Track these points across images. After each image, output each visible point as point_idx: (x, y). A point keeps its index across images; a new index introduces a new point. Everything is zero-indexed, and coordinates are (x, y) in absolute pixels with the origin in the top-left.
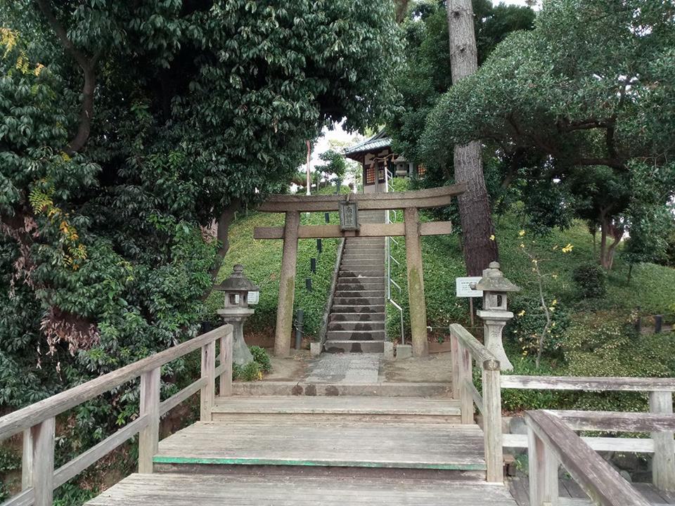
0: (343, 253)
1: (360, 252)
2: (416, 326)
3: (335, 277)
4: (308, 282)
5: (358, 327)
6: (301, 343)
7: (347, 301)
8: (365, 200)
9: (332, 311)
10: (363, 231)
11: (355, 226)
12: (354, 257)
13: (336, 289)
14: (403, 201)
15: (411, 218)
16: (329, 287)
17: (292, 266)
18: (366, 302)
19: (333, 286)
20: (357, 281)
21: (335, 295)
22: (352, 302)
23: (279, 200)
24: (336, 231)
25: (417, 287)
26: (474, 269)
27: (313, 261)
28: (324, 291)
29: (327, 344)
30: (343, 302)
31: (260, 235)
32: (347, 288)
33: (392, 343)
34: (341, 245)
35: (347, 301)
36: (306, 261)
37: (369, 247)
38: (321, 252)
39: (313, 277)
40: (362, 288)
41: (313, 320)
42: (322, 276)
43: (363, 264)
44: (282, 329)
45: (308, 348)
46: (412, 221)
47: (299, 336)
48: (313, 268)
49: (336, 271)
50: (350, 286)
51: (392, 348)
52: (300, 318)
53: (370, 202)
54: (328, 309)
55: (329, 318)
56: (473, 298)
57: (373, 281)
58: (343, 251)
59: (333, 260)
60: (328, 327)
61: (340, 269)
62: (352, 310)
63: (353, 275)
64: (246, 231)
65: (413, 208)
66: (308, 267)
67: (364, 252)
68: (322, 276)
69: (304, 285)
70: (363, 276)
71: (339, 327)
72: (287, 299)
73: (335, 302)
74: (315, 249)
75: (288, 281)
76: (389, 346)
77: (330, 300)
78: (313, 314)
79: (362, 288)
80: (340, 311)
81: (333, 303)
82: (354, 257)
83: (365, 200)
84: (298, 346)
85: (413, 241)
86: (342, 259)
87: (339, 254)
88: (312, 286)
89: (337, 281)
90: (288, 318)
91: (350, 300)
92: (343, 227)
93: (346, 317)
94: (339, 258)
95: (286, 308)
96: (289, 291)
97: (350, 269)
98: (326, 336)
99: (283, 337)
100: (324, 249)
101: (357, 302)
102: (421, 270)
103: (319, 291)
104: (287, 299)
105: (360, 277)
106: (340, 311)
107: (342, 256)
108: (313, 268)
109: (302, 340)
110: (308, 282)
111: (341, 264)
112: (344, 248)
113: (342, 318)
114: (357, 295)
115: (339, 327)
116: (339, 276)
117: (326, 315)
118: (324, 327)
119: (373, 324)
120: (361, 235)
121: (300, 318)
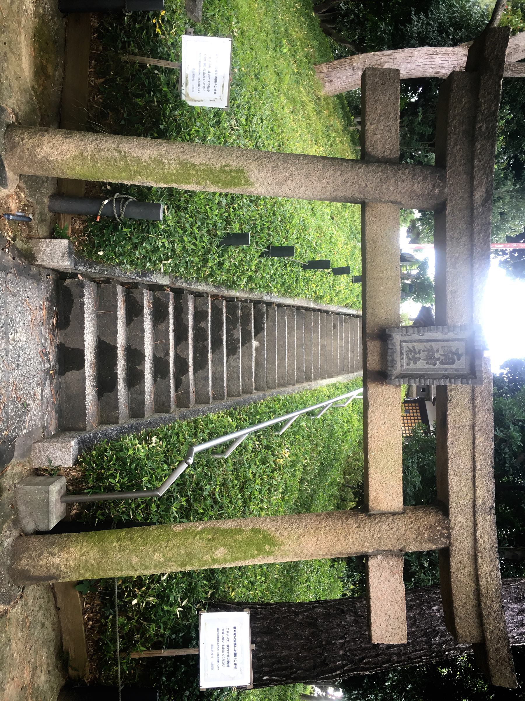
0: (299, 308)
1: (300, 339)
2: (104, 553)
3: (256, 295)
4: (240, 239)
5: (134, 355)
7: (203, 325)
8: (473, 399)
9: (179, 293)
12: (291, 329)
13: (230, 300)
14: (469, 510)
15: (420, 534)
16: (232, 285)
18: (200, 363)
19: (234, 293)
20: (246, 339)
21: (215, 297)
22: (200, 335)
23: (478, 145)
24: (380, 315)
27: (289, 251)
28: (222, 276)
29: (81, 285)
30: (199, 316)
31: (374, 90)
32: (232, 322)
34: (312, 305)
35: (203, 325)
36: (286, 238)
37: (308, 354)
38: (305, 267)
39: (254, 251)
40: (232, 350)
41: (135, 247)
42: (256, 271)
45: (54, 234)
49: (267, 298)
50: (235, 327)
51: (56, 463)
52: (137, 213)
53: (468, 414)
54: (181, 284)
55: (161, 288)
56: (198, 656)
57: (247, 370)
58: (302, 307)
59: (288, 291)
60: (135, 285)
61: (269, 304)
63: (258, 330)
64: (334, 137)
65: (449, 537)
66: (277, 241)
67: (300, 346)
68: (256, 271)
69: (236, 228)
70: (256, 350)
71: (134, 312)
72: (182, 164)
73: (200, 300)
74: (310, 256)
77: (202, 287)
78: (155, 250)
79: (232, 350)
80: (180, 311)
81: (198, 295)
82: (291, 329)
86: (288, 306)
89: (245, 301)
92: (397, 337)
93: (161, 327)
94: (289, 301)
95: (156, 161)
96: (210, 174)
97: (270, 324)
98: (107, 281)
99: (67, 154)
100: (309, 274)
102: (270, 560)
103: (220, 265)
104: (182, 164)
105: (255, 344)
106: (180, 311)
107: (294, 306)
109: (79, 215)
110: (240, 239)
111: (279, 305)
112: (307, 309)
113: (159, 316)
114: (217, 343)
115: (134, 312)
116: (257, 303)
117: (164, 281)
118: (128, 273)
120: (372, 388)
121: (137, 213)
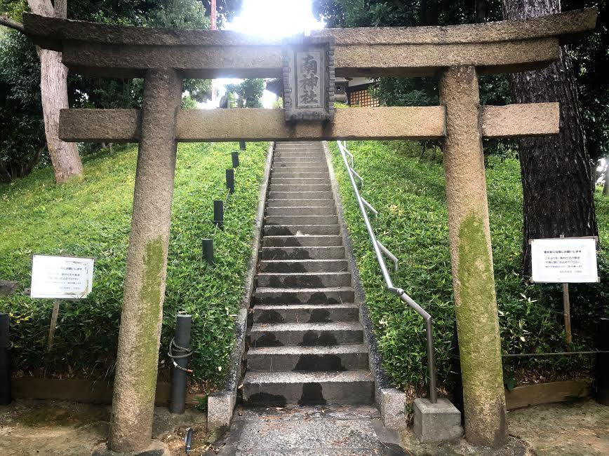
0: (268, 197)
1: (294, 196)
2: (480, 365)
3: (256, 234)
4: (207, 247)
5: (309, 339)
6: (185, 396)
7: (282, 280)
8: (347, 45)
9: (255, 301)
10: (340, 127)
11: (322, 111)
12: (286, 204)
13: (260, 256)
14: (443, 48)
16: (248, 255)
17: (160, 212)
18: (316, 282)
19: (255, 253)
20: (294, 242)
21: (258, 269)
22: (291, 283)
23: (126, 41)
24: (274, 126)
25: (480, 265)
26: (548, 222)
27: (218, 205)
29: (248, 385)
30: (274, 283)
31: (78, 131)
32: (281, 254)
33: (403, 396)
34: (265, 185)
35: (282, 280)
36: (207, 207)
38: (232, 191)
41: (215, 338)
42: (236, 234)
43: (300, 214)
44: (128, 377)
45: (203, 409)
46: (466, 99)
47: (180, 381)
48: (218, 218)
49: (259, 224)
50: (284, 252)
51: (402, 407)
52: (185, 337)
54: (247, 299)
55: (250, 316)
56: (569, 284)
58: (267, 193)
59: (253, 206)
60: (248, 338)
61: (264, 222)
62: (292, 299)
63: (286, 231)
64: (120, 166)
65: (467, 66)
68: (236, 234)
69: (198, 251)
73: (261, 283)
74: (222, 187)
75: (149, 248)
76: (394, 400)
77: (250, 281)
78: (217, 321)
80: (270, 300)
81: (256, 284)
82: (286, 204)
83: (347, 45)
84: (178, 404)
85: (467, 150)
86: (266, 206)
87: (262, 198)
88: (216, 255)
89: (261, 243)
90: (146, 346)
91: (287, 278)
92: (293, 111)
93: (284, 316)
96: (152, 273)
100: (238, 188)
101: (299, 282)
103: (230, 265)
105: (298, 235)
106: (270, 300)
107: (266, 201)
108: (218, 218)
110: (207, 247)
111: (265, 214)
112: (269, 189)
113: (274, 318)
115: (270, 340)
116: (263, 233)
118: (237, 344)
119: (341, 332)
120: (337, 132)
121: (185, 337)
